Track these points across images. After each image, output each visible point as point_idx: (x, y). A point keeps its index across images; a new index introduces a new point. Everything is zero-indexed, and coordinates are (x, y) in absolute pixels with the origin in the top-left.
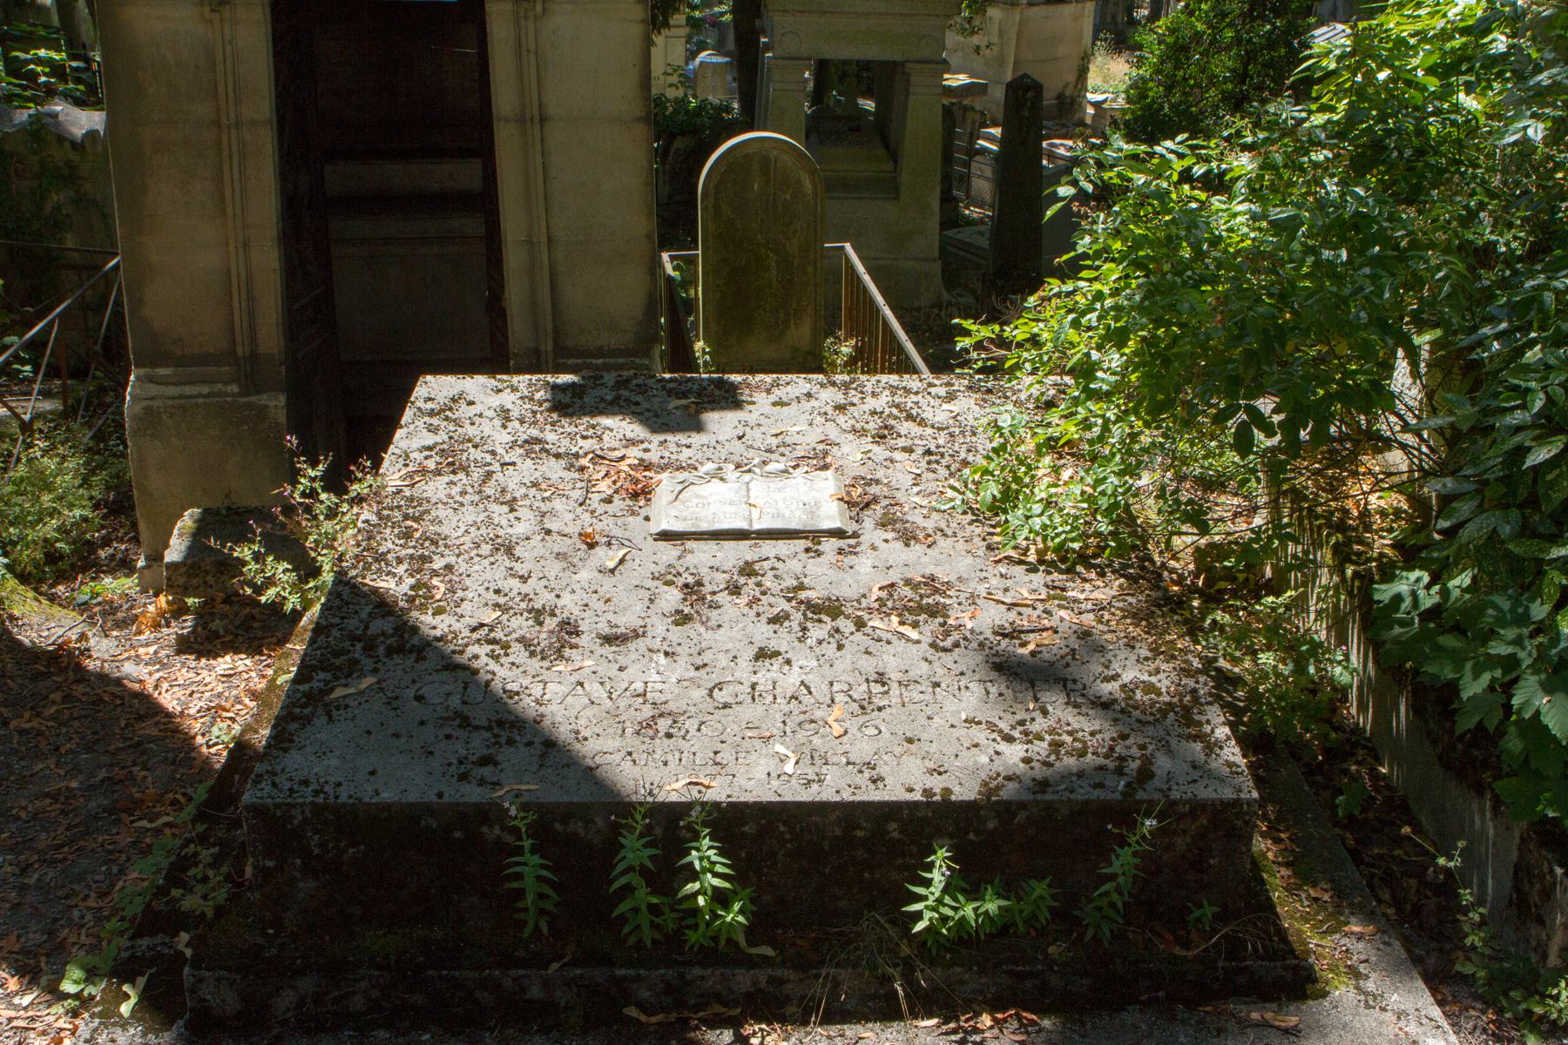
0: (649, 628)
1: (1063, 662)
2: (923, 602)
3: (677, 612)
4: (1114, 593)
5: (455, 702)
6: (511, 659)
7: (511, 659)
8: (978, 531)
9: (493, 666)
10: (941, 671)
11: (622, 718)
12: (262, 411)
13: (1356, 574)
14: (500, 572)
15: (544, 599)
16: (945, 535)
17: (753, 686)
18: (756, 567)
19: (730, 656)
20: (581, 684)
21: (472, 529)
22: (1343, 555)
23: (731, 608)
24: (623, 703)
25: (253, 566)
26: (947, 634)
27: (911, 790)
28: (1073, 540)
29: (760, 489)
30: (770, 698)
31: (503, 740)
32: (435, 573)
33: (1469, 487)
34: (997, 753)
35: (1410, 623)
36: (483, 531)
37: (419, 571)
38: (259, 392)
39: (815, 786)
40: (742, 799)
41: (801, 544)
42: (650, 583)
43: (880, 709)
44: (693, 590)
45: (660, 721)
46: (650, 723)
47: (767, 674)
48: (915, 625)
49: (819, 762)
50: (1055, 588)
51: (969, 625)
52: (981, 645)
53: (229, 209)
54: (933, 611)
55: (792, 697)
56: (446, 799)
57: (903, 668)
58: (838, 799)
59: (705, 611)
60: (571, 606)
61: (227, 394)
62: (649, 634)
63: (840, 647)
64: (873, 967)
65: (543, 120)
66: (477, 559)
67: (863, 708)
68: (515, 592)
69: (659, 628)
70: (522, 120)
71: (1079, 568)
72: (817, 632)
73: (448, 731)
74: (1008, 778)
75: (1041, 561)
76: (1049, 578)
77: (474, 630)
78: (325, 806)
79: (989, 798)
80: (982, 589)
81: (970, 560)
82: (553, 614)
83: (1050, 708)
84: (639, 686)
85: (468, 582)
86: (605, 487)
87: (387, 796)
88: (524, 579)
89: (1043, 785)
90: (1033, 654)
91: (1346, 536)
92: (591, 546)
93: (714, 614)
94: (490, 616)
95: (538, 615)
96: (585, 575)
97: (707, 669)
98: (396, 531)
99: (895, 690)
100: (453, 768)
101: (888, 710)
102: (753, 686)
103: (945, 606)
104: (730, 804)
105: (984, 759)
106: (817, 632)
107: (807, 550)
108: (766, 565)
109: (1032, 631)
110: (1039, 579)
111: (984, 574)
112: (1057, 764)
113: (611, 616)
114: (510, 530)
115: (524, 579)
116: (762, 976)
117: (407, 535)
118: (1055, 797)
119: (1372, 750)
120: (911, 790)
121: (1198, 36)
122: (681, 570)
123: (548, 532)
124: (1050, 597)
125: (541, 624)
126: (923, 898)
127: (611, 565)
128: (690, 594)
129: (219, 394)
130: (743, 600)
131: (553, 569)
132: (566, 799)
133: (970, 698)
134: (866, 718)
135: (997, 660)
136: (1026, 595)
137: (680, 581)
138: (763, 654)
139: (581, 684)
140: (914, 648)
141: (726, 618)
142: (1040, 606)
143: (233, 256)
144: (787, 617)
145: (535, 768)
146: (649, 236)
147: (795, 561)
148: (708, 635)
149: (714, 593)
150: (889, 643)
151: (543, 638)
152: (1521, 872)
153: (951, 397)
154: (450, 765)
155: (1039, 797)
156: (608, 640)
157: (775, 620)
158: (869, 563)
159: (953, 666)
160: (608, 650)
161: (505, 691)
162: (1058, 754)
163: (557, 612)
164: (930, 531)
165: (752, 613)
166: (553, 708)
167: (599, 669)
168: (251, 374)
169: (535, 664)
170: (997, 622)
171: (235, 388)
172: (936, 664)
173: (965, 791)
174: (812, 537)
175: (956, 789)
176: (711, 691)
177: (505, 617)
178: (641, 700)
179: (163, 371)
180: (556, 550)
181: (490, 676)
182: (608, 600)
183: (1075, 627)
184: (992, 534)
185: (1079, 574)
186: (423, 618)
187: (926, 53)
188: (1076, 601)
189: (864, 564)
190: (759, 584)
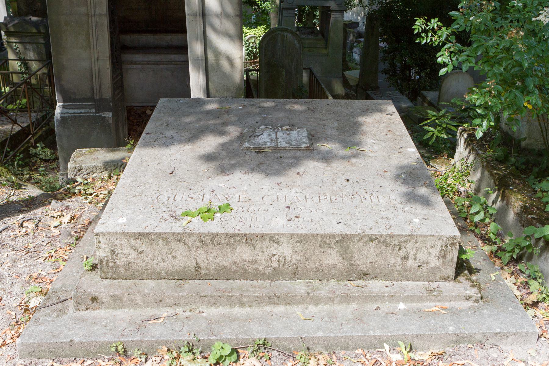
53: (92, 46)
61: (91, 113)
143: (93, 63)
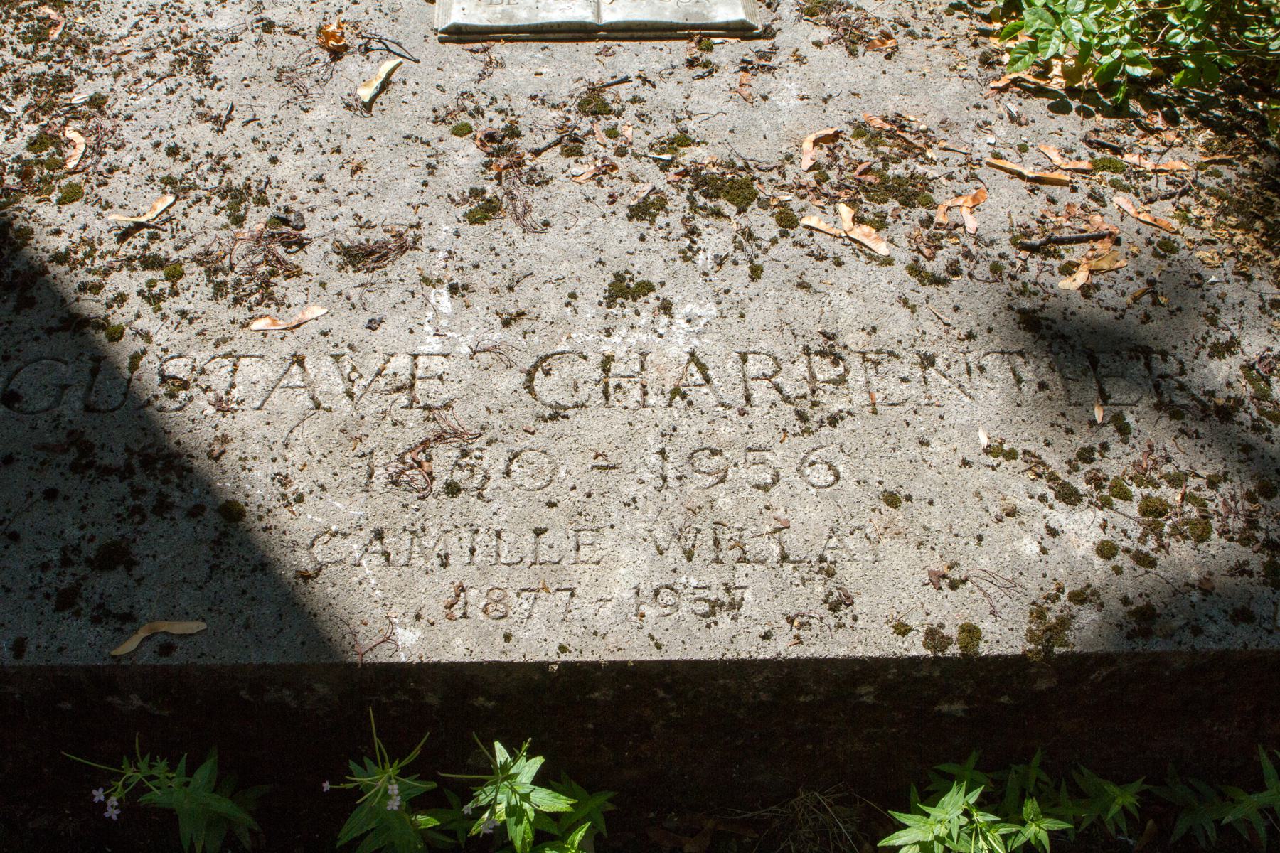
0: (425, 230)
1: (1138, 310)
2: (885, 174)
3: (477, 193)
4: (1197, 158)
5: (72, 406)
6: (181, 303)
7: (181, 303)
8: (964, 26)
9: (149, 322)
10: (933, 330)
11: (369, 444)
14: (183, 109)
15: (250, 166)
16: (911, 34)
17: (606, 363)
18: (608, 97)
19: (565, 291)
20: (299, 361)
21: (147, 21)
23: (568, 181)
24: (371, 406)
26: (935, 244)
27: (902, 630)
28: (1135, 62)
30: (636, 393)
31: (147, 502)
32: (74, 113)
34: (1053, 532)
36: (163, 26)
37: (46, 109)
39: (724, 619)
40: (588, 657)
41: (681, 50)
42: (430, 131)
43: (834, 421)
44: (499, 145)
45: (434, 460)
48: (880, 224)
49: (730, 555)
50: (1102, 146)
51: (971, 223)
52: (996, 269)
54: (912, 193)
55: (676, 391)
56: (31, 658)
57: (870, 321)
58: (767, 654)
59: (522, 191)
60: (293, 179)
62: (425, 243)
63: (756, 273)
66: (147, 82)
67: (802, 417)
68: (202, 151)
69: (443, 226)
71: (1135, 106)
72: (715, 239)
73: (51, 479)
74: (1079, 598)
75: (1072, 92)
76: (1090, 124)
77: (125, 235)
79: (1048, 650)
80: (982, 145)
81: (955, 85)
82: (262, 201)
83: (1130, 419)
84: (400, 363)
85: (126, 131)
88: (220, 124)
89: (1143, 618)
90: (1086, 290)
92: (337, 54)
93: (536, 197)
94: (155, 204)
95: (236, 200)
96: (323, 113)
97: (525, 324)
98: (23, 26)
99: (857, 376)
100: (50, 576)
101: (848, 424)
102: (606, 363)
103: (926, 182)
104: (565, 665)
105: (1029, 547)
106: (715, 239)
107: (691, 63)
108: (624, 91)
109: (1078, 240)
110: (1073, 126)
111: (983, 115)
112: (1162, 559)
113: (359, 204)
114: (207, 24)
115: (220, 124)
117: (38, 36)
118: (1169, 646)
120: (902, 630)
122: (483, 103)
123: (268, 26)
124: (1098, 166)
125: (239, 221)
127: (365, 94)
128: (497, 154)
130: (586, 168)
131: (272, 98)
132: (255, 658)
133: (985, 402)
134: (809, 442)
135: (1026, 303)
136: (1057, 160)
137: (481, 126)
138: (623, 290)
139: (299, 361)
140: (882, 274)
141: (557, 205)
142: (1080, 182)
144: (661, 205)
145: (200, 574)
147: (672, 84)
148: (526, 244)
149: (537, 153)
150: (839, 263)
151: (241, 256)
154: (45, 567)
155: (1139, 645)
156: (355, 256)
157: (641, 211)
158: (793, 88)
159: (953, 318)
160: (350, 280)
161: (164, 379)
162: (1155, 529)
163: (270, 194)
164: (887, 27)
165: (602, 196)
166: (247, 418)
167: (334, 324)
169: (222, 314)
170: (1018, 219)
172: (924, 312)
173: (1005, 636)
175: (987, 626)
176: (530, 375)
177: (181, 205)
178: (403, 399)
180: (278, 63)
181: (140, 344)
182: (358, 168)
183: (1147, 231)
184: (986, 33)
185: (1135, 116)
186: (41, 210)
188: (1141, 174)
189: (785, 88)
190: (612, 133)
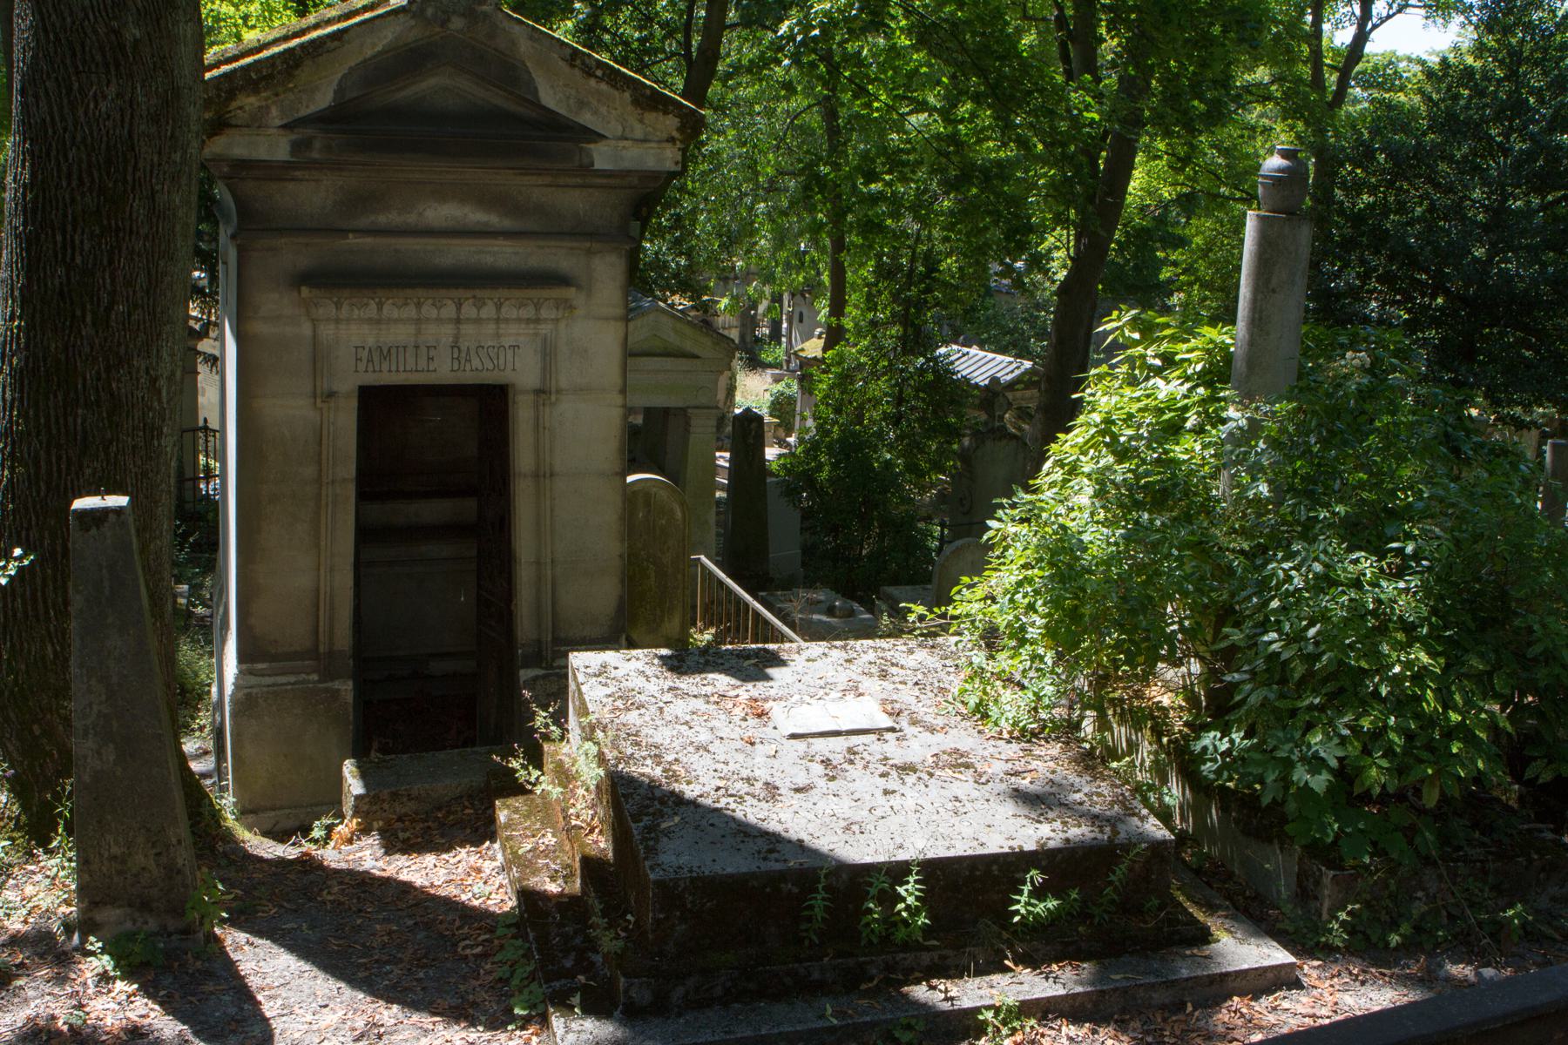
12: (335, 694)
13: (1170, 741)
22: (1157, 732)
25: (522, 772)
29: (834, 708)
33: (1246, 676)
35: (1215, 760)
38: (332, 680)
41: (873, 737)
46: (847, 828)
47: (895, 801)
64: (992, 945)
65: (552, 475)
70: (537, 476)
78: (698, 878)
86: (738, 711)
87: (729, 870)
91: (1156, 720)
110: (1015, 746)
116: (935, 955)
119: (1195, 841)
121: (860, 366)
126: (1018, 902)
129: (302, 682)
146: (621, 556)
152: (1302, 876)
153: (911, 651)
160: (798, 795)
168: (327, 665)
171: (315, 677)
174: (879, 732)
179: (260, 666)
187: (703, 400)
